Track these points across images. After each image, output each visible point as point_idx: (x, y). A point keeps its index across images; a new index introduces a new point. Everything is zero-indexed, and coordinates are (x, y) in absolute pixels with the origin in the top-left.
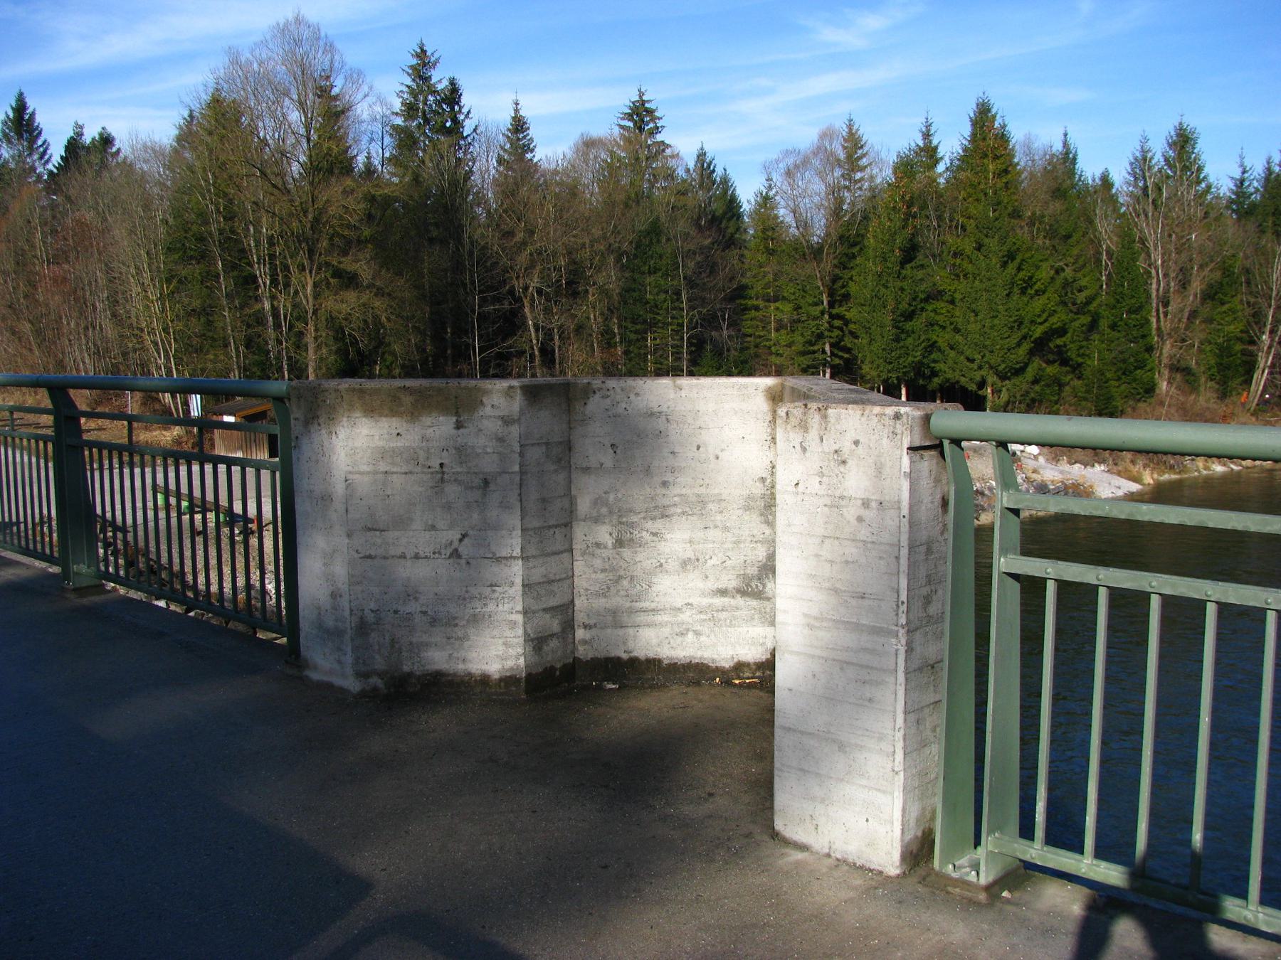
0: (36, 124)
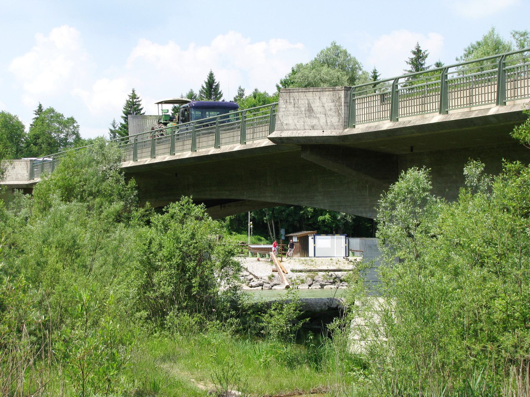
0: (220, 91)
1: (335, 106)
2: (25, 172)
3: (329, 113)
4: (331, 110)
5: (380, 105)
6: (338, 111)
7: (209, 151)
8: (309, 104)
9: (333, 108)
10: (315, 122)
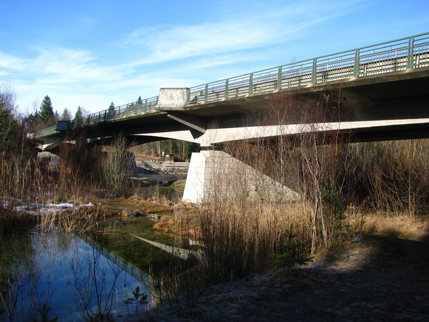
2: (66, 125)
4: (180, 97)
8: (171, 94)
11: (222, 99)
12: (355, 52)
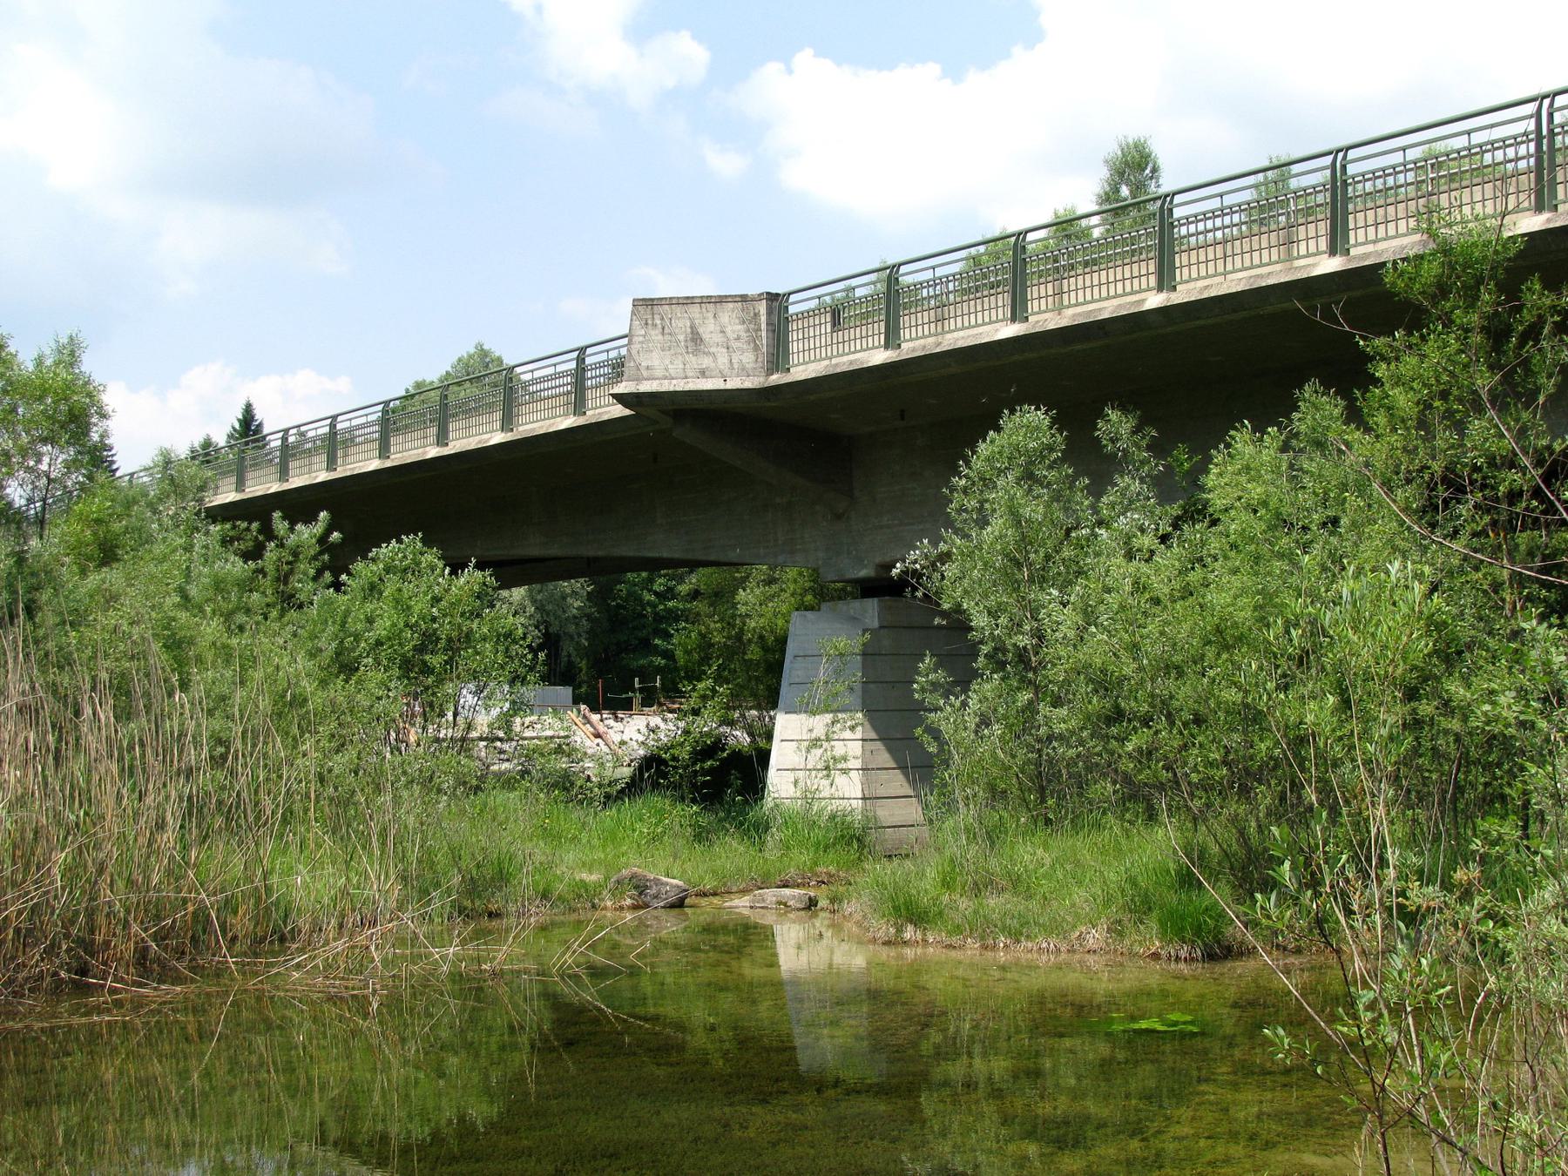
1: (748, 331)
3: (735, 345)
4: (738, 338)
5: (832, 332)
6: (754, 342)
7: (425, 453)
9: (743, 334)
10: (706, 362)
11: (1314, 265)
12: (1530, 108)
